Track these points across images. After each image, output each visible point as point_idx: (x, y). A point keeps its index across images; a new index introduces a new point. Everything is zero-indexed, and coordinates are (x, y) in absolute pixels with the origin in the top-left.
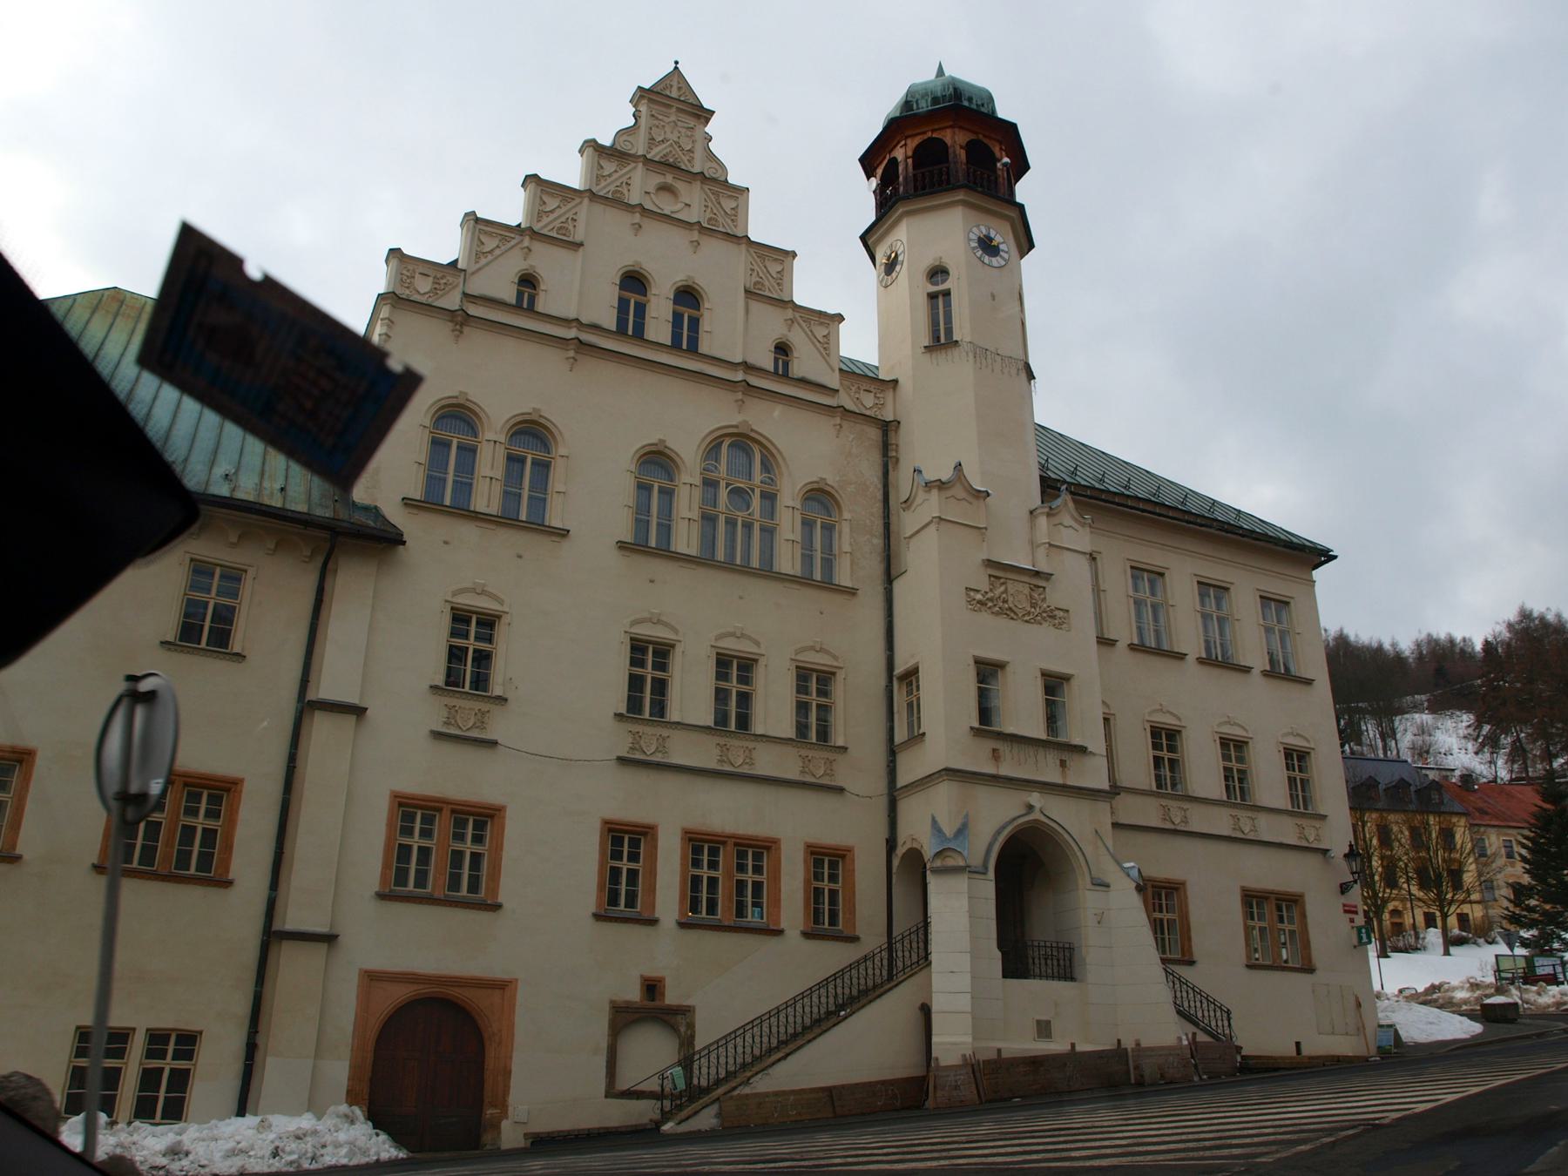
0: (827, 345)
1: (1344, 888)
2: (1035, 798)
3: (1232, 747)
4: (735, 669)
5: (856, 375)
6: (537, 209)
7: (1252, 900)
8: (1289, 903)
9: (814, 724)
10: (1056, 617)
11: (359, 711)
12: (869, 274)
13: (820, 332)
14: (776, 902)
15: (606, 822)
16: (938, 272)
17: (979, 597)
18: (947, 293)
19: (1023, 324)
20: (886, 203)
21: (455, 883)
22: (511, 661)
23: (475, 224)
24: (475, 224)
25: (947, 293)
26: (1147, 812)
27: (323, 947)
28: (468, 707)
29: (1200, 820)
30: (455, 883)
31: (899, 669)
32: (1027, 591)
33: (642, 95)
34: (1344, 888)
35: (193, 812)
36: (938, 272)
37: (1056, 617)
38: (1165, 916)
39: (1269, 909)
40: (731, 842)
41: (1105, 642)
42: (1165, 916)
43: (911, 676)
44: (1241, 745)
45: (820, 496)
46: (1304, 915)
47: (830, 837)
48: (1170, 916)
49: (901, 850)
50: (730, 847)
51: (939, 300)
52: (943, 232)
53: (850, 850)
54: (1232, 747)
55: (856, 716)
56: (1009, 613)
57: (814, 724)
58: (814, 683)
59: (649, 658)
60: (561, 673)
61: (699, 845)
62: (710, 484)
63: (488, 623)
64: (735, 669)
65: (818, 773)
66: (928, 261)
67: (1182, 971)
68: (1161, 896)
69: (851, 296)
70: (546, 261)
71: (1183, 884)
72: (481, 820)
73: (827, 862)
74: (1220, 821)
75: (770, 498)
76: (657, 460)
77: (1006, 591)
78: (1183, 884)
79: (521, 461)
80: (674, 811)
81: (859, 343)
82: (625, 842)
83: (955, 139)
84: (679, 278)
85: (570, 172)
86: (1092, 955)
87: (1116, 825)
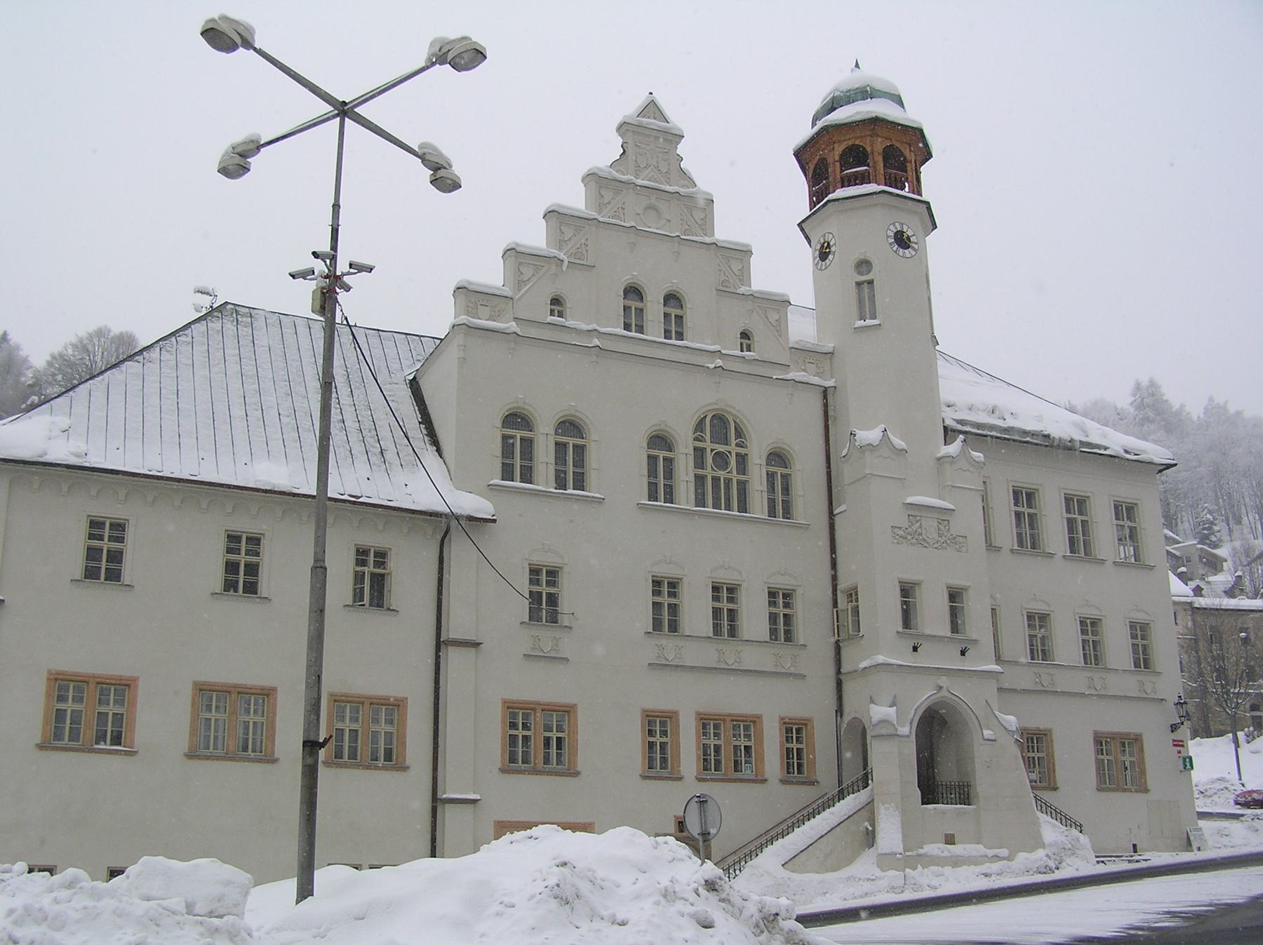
0: (780, 328)
1: (1174, 728)
2: (944, 681)
3: (1090, 626)
4: (724, 593)
5: (804, 353)
6: (557, 238)
7: (1101, 742)
8: (1131, 742)
9: (782, 627)
10: (957, 542)
11: (476, 645)
12: (806, 254)
13: (773, 317)
14: (761, 759)
15: (505, 702)
16: (864, 265)
17: (901, 533)
18: (871, 282)
19: (929, 299)
20: (818, 195)
21: (547, 760)
22: (570, 596)
23: (513, 254)
24: (513, 254)
25: (871, 282)
26: (1024, 678)
27: (470, 807)
28: (546, 636)
29: (1065, 681)
30: (547, 760)
31: (843, 585)
32: (935, 524)
33: (623, 128)
34: (1174, 728)
35: (343, 719)
36: (864, 265)
37: (957, 542)
38: (1036, 755)
39: (1115, 747)
40: (539, 709)
41: (991, 547)
42: (1036, 755)
43: (852, 594)
44: (1095, 623)
45: (778, 458)
46: (1142, 750)
47: (796, 711)
48: (1040, 755)
49: (847, 718)
50: (367, 706)
51: (865, 287)
52: (864, 221)
53: (676, 713)
54: (1090, 626)
55: (812, 621)
56: (923, 543)
57: (782, 627)
58: (780, 598)
59: (665, 589)
60: (607, 607)
61: (706, 723)
62: (699, 453)
63: (553, 574)
64: (724, 593)
65: (787, 666)
66: (856, 256)
67: (1047, 796)
68: (1034, 744)
69: (783, 266)
70: (573, 287)
71: (1050, 731)
72: (208, 695)
73: (794, 730)
74: (1078, 681)
75: (742, 460)
76: (660, 440)
77: (921, 527)
78: (1050, 731)
79: (565, 445)
80: (689, 699)
81: (802, 329)
82: (658, 726)
83: (876, 146)
84: (665, 288)
85: (576, 199)
86: (982, 784)
87: (1000, 690)
